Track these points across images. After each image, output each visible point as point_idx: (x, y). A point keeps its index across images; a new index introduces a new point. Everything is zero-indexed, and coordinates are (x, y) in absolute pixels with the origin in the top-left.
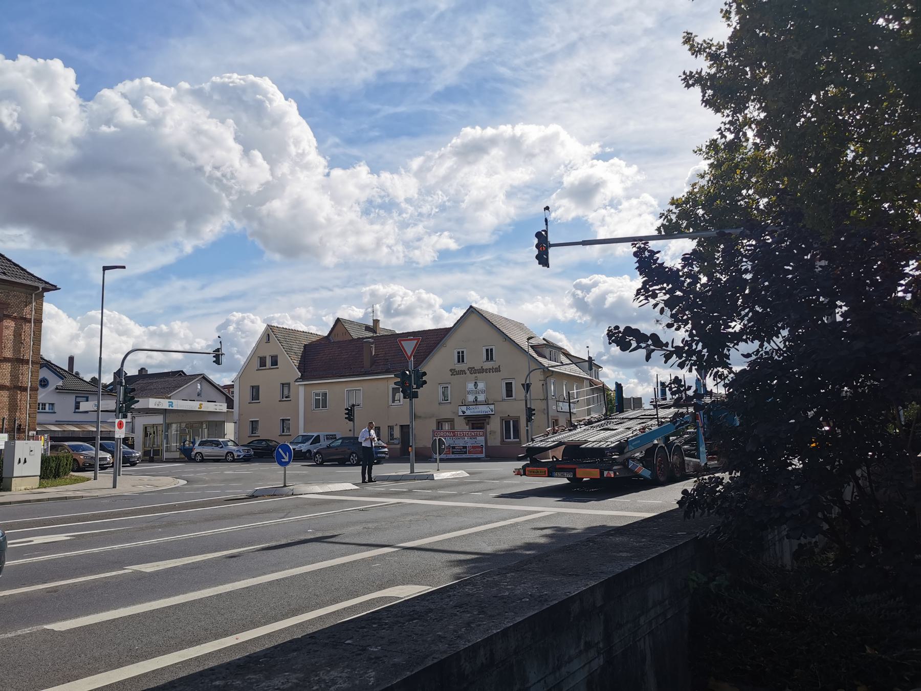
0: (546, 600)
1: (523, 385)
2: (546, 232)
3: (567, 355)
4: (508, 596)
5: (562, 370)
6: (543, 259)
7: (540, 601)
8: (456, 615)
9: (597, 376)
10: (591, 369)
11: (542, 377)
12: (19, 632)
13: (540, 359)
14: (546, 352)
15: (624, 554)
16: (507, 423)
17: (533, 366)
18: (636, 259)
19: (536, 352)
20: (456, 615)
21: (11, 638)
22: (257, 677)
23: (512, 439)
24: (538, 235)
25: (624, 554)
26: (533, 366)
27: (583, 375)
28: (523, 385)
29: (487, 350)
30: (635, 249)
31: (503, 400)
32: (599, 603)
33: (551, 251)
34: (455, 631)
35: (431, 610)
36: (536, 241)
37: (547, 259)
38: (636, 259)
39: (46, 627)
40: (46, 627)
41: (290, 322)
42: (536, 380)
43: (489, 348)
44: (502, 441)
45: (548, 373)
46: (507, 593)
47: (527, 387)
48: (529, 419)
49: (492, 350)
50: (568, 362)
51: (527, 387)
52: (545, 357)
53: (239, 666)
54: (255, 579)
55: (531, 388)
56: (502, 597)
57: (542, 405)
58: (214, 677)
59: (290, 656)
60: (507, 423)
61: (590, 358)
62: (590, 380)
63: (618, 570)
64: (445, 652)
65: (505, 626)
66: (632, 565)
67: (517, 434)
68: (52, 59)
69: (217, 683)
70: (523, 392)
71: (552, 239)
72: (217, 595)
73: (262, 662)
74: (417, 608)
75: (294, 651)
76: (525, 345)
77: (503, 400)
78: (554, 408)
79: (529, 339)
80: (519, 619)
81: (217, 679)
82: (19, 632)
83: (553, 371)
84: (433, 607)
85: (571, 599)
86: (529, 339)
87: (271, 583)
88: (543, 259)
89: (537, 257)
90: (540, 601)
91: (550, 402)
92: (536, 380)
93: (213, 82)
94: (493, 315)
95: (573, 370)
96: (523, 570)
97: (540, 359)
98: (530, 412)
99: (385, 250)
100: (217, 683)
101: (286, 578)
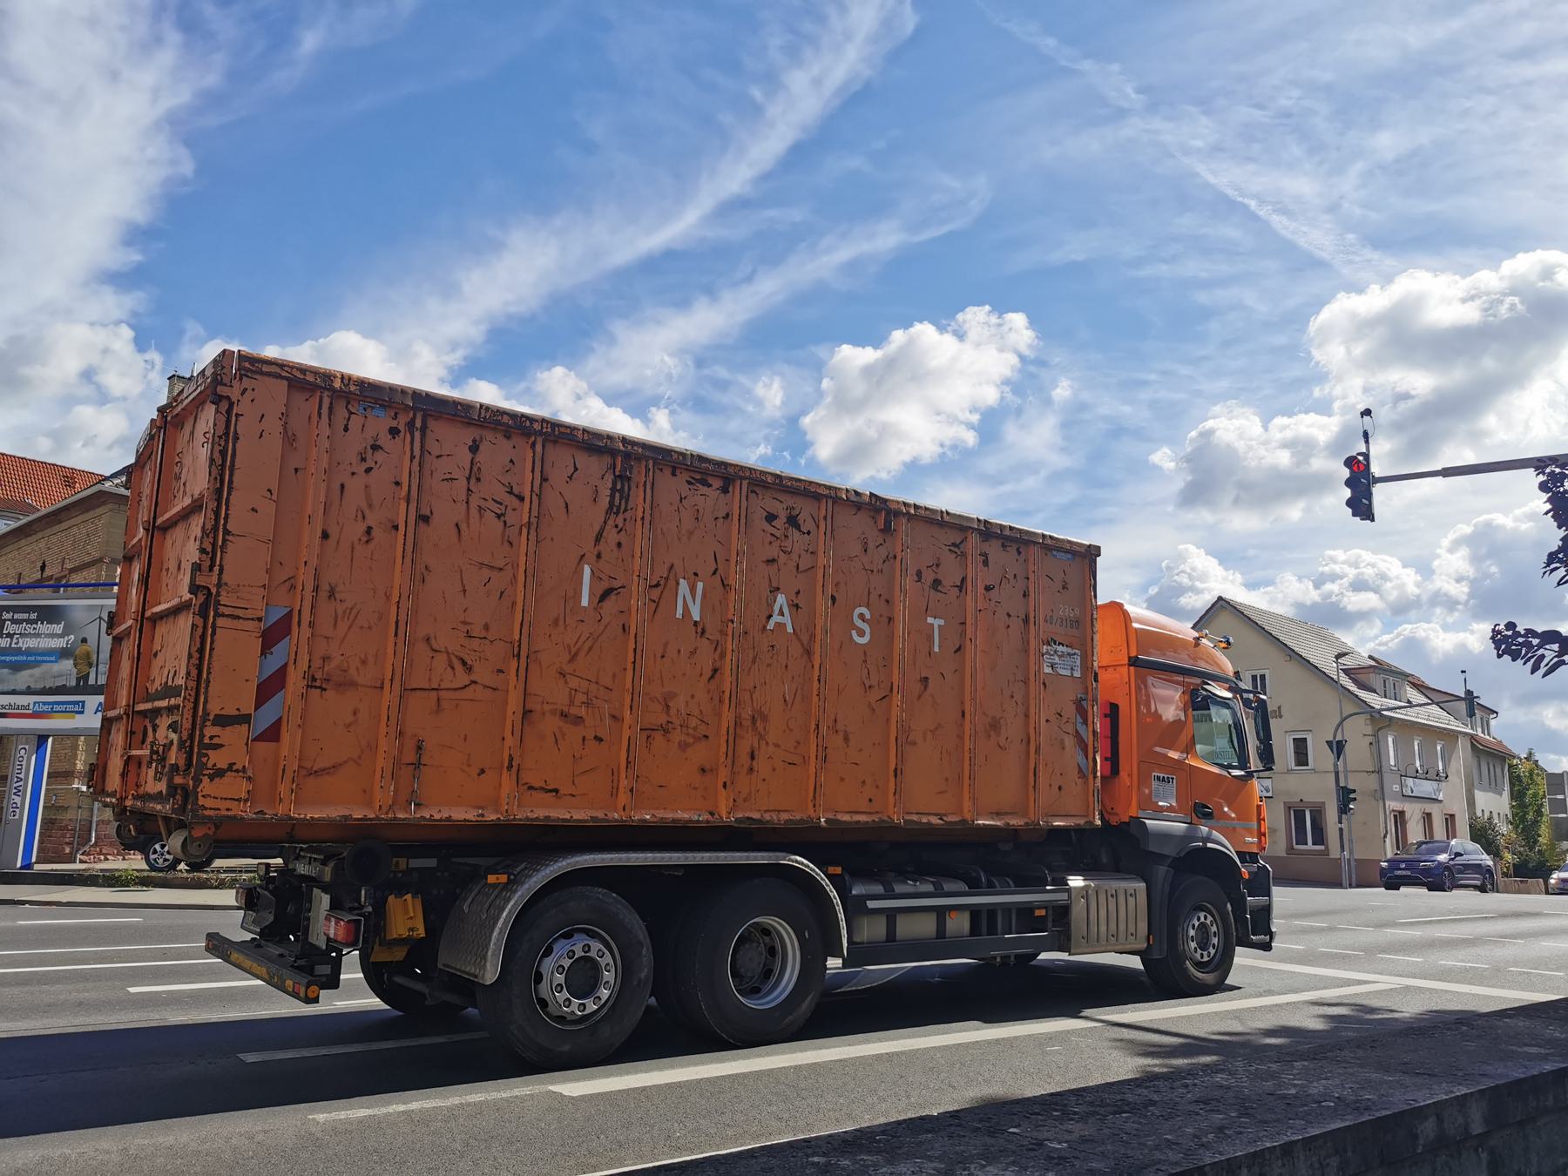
0: (1367, 1109)
3: (1420, 687)
4: (1295, 1096)
6: (1361, 506)
7: (1357, 1109)
9: (1486, 727)
10: (1471, 714)
11: (1369, 730)
12: (516, 1092)
13: (1363, 694)
14: (1376, 680)
15: (1534, 1050)
16: (1300, 817)
17: (1349, 708)
18: (1545, 496)
19: (1355, 681)
21: (506, 1100)
22: (874, 1158)
23: (1310, 846)
25: (1534, 1050)
26: (1349, 708)
27: (1455, 725)
29: (1254, 678)
30: (1542, 478)
31: (1290, 771)
32: (1477, 1128)
33: (1378, 491)
34: (1195, 1136)
35: (1153, 1103)
36: (1346, 473)
37: (1370, 506)
38: (1545, 496)
39: (551, 1088)
40: (551, 1088)
41: (105, 1145)
42: (1357, 733)
43: (1258, 673)
44: (1290, 849)
45: (1380, 722)
46: (1293, 1091)
47: (1338, 747)
48: (1344, 810)
49: (1263, 677)
51: (1338, 747)
53: (845, 1141)
54: (852, 1048)
55: (1347, 748)
56: (1284, 1097)
57: (1371, 782)
59: (923, 1137)
61: (1469, 693)
62: (1472, 737)
63: (1519, 1074)
64: (1177, 1164)
66: (1548, 1067)
67: (1320, 837)
69: (816, 1159)
70: (1330, 757)
71: (1376, 470)
74: (1129, 1097)
75: (929, 1131)
76: (1331, 668)
77: (1290, 771)
79: (1338, 656)
81: (815, 1154)
82: (516, 1092)
83: (1391, 718)
84: (1156, 1097)
85: (1419, 1113)
86: (1338, 656)
87: (878, 1058)
88: (1361, 506)
89: (1349, 503)
90: (1357, 1109)
91: (1387, 778)
92: (1357, 733)
95: (1433, 716)
97: (1363, 694)
98: (1345, 797)
99: (232, 746)
100: (816, 1159)
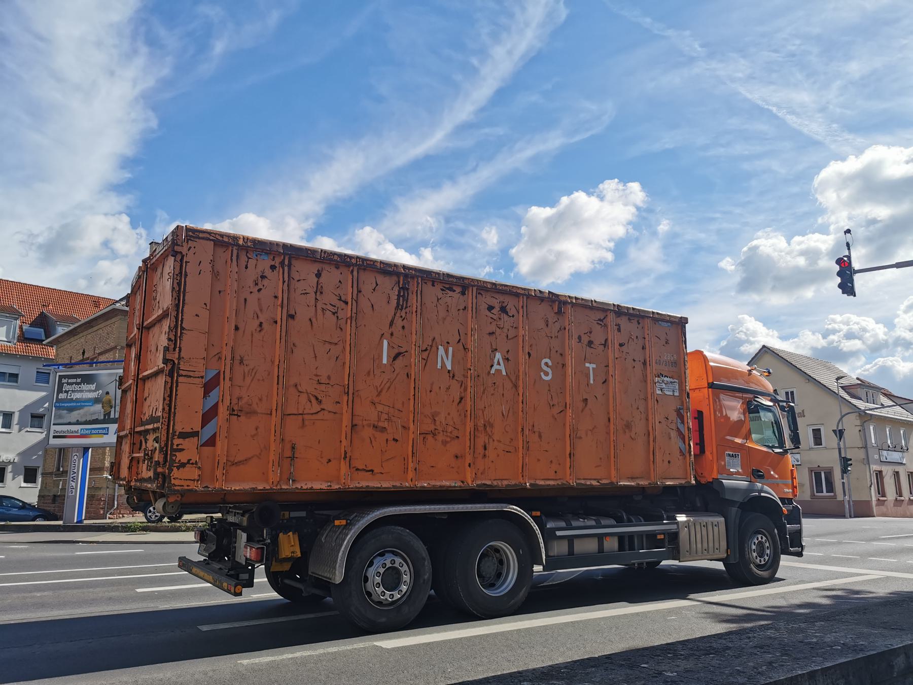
0: (861, 650)
1: (834, 431)
2: (849, 257)
3: (888, 395)
4: (816, 643)
5: (883, 413)
6: (847, 287)
7: (855, 650)
8: (756, 654)
11: (858, 422)
12: (355, 646)
13: (854, 401)
14: (861, 392)
16: (818, 476)
19: (848, 393)
20: (756, 654)
23: (825, 493)
24: (839, 261)
28: (834, 431)
31: (811, 449)
33: (857, 277)
34: (754, 668)
35: (729, 648)
44: (813, 495)
45: (865, 417)
46: (815, 640)
47: (840, 434)
48: (844, 471)
49: (792, 393)
50: (892, 403)
51: (840, 434)
52: (860, 399)
53: (543, 673)
56: (810, 643)
57: (861, 454)
58: (522, 679)
60: (818, 476)
65: (811, 669)
67: (831, 488)
68: (602, 182)
70: (835, 439)
71: (856, 265)
72: (517, 630)
73: (563, 673)
74: (714, 645)
75: (592, 667)
76: (834, 386)
77: (811, 449)
78: (876, 457)
79: (838, 379)
80: (828, 664)
82: (355, 646)
83: (871, 415)
84: (730, 645)
85: (893, 652)
86: (838, 379)
88: (847, 287)
89: (840, 286)
92: (851, 425)
93: (824, 230)
94: (792, 354)
96: (835, 620)
97: (854, 401)
98: (845, 463)
101: (581, 621)
